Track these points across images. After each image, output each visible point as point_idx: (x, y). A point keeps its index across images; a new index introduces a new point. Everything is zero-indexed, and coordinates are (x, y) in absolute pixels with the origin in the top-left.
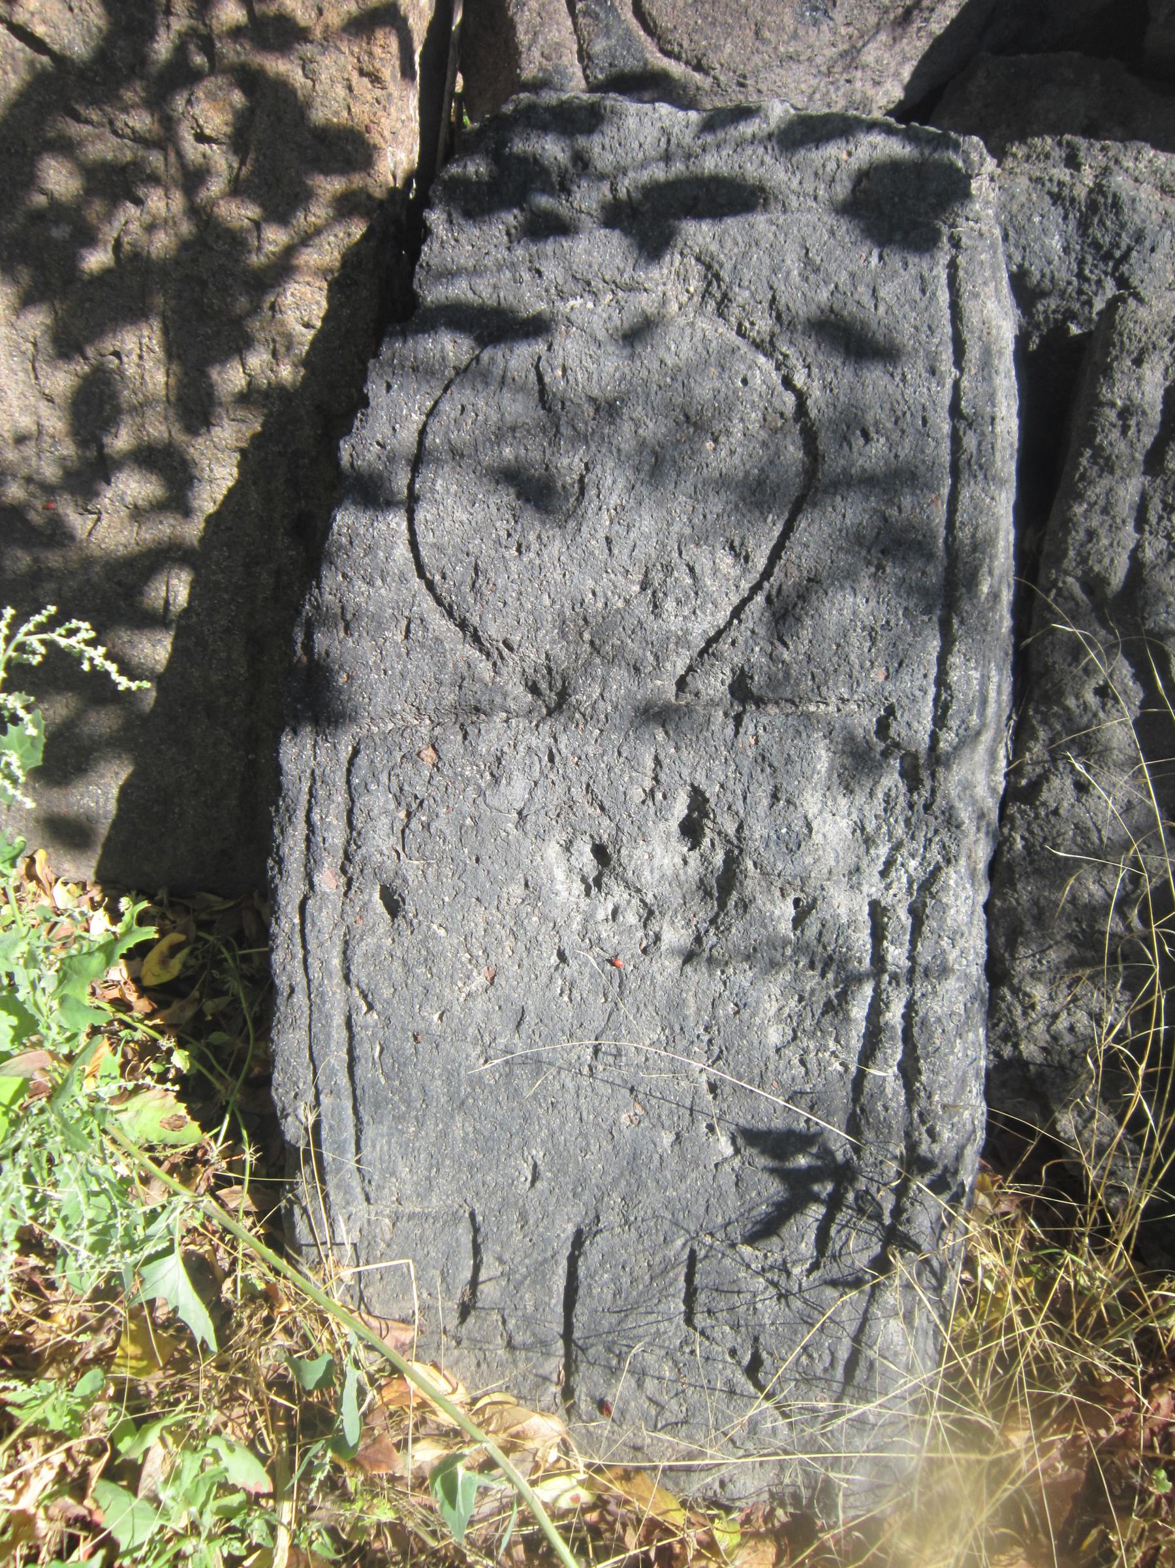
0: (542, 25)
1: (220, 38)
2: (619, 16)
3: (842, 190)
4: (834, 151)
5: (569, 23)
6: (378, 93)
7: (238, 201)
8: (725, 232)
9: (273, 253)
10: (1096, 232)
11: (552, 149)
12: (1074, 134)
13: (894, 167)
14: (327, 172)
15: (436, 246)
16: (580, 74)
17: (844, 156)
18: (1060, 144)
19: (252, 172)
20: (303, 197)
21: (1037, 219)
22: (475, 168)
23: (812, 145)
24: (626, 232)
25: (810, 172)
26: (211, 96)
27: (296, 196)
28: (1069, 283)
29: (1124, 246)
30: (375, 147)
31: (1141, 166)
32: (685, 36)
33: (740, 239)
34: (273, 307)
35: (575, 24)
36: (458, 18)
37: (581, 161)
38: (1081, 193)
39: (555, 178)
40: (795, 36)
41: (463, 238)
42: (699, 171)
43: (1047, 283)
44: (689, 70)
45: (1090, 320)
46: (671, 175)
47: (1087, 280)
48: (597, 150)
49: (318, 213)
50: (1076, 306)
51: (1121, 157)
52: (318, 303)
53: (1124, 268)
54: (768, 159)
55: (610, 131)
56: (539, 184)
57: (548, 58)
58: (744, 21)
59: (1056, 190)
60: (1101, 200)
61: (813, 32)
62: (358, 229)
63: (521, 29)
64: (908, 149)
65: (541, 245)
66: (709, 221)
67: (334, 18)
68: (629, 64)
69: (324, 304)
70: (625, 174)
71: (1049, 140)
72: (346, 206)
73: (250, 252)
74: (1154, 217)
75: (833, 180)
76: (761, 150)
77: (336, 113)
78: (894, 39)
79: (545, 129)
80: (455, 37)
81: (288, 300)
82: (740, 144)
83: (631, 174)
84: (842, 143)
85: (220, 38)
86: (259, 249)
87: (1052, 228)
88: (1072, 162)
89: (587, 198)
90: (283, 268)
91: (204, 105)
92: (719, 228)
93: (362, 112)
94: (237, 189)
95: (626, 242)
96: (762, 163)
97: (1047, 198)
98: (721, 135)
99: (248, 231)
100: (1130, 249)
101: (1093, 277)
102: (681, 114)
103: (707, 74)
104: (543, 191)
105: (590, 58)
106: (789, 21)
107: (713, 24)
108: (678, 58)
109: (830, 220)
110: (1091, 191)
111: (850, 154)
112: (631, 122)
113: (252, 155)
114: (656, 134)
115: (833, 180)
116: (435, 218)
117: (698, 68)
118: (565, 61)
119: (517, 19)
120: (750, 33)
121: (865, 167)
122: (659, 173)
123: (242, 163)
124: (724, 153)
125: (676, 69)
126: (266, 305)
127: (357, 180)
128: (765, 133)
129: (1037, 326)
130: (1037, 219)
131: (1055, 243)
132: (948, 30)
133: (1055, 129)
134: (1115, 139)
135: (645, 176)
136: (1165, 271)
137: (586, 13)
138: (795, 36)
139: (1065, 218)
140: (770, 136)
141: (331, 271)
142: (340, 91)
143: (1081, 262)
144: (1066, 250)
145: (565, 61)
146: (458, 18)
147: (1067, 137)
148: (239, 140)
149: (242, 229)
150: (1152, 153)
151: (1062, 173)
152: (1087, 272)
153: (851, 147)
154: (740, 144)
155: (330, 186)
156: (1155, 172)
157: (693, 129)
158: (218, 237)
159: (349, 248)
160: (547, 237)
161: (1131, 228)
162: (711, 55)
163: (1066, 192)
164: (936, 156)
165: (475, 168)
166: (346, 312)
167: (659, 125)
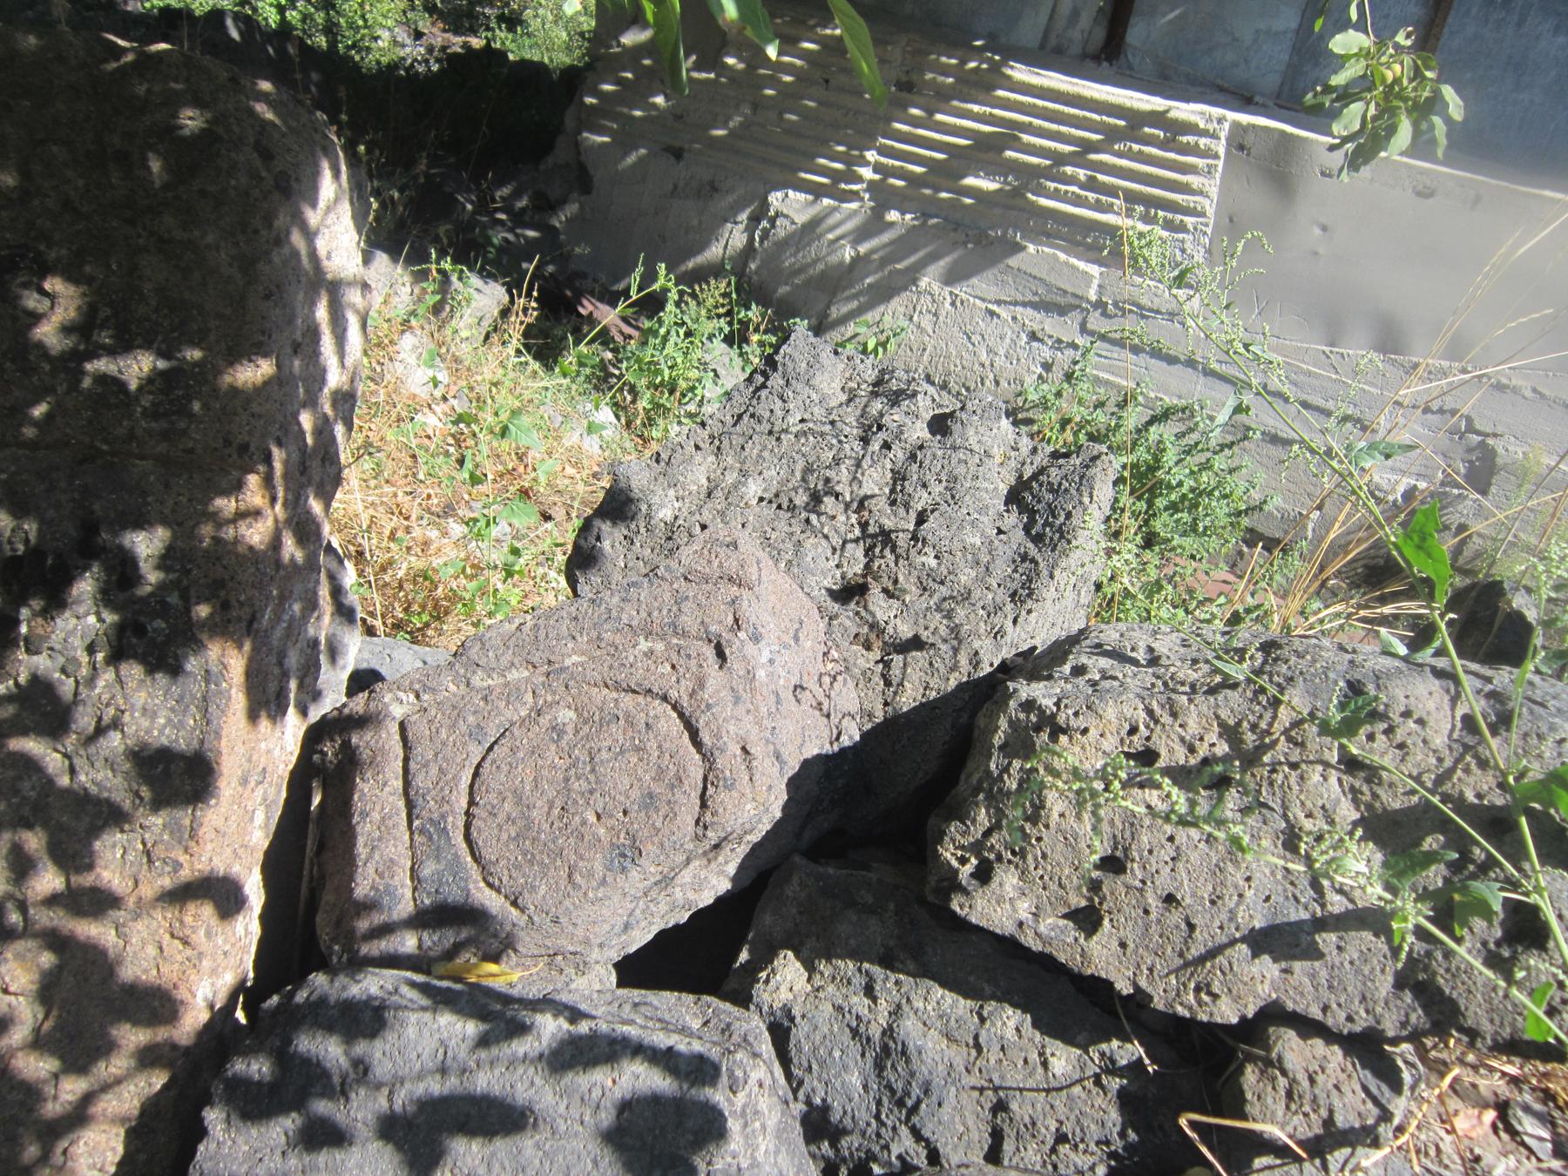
0: (380, 839)
1: (35, 905)
2: (449, 839)
3: (607, 1118)
4: (600, 1077)
5: (407, 837)
6: (189, 952)
7: (37, 1054)
8: (493, 1154)
9: (70, 1103)
10: (889, 1073)
11: (331, 1051)
12: (872, 962)
13: (654, 1101)
14: (136, 1023)
15: (213, 1146)
16: (408, 894)
17: (610, 1083)
18: (860, 970)
19: (54, 1028)
20: (106, 1048)
21: (837, 1054)
22: (257, 1068)
23: (580, 1068)
24: (399, 1147)
25: (577, 1097)
26: (19, 957)
27: (98, 1049)
28: (868, 1124)
29: (914, 1098)
30: (182, 1002)
31: (929, 1008)
32: (506, 872)
33: (507, 1163)
34: (65, 1152)
35: (412, 840)
36: (316, 800)
37: (362, 1068)
38: (875, 1032)
39: (336, 1080)
40: (603, 882)
41: (240, 1140)
42: (472, 1088)
43: (848, 1122)
44: (508, 904)
45: (890, 1163)
46: (446, 1091)
47: (884, 1124)
48: (378, 1055)
49: (118, 1064)
50: (876, 1149)
51: (913, 996)
52: (113, 1149)
53: (915, 1119)
54: (538, 1081)
55: (391, 1036)
56: (319, 1089)
57: (381, 876)
58: (559, 863)
59: (854, 1024)
60: (892, 1045)
61: (620, 878)
62: (158, 1080)
63: (361, 841)
64: (668, 1081)
65: (313, 1156)
66: (480, 1140)
67: (147, 891)
68: (453, 894)
69: (120, 1150)
70: (402, 1084)
71: (851, 965)
72: (148, 1058)
73: (45, 1100)
74: (940, 1068)
75: (598, 1107)
76: (532, 1070)
77: (146, 971)
78: (709, 861)
79: (330, 1028)
80: (313, 816)
81: (80, 1149)
82: (512, 1063)
83: (408, 1085)
84: (606, 1069)
85: (35, 905)
86: (55, 1098)
87: (852, 1064)
88: (869, 991)
89: (361, 1111)
90: (79, 1116)
91: (12, 965)
92: (487, 1151)
93: (169, 974)
94: (38, 1043)
95: (397, 1158)
96: (532, 1083)
97: (847, 1030)
98: (495, 1051)
99: (45, 1082)
100: (919, 1102)
101: (889, 1123)
102: (459, 1025)
103: (523, 911)
104: (323, 1095)
105: (419, 881)
106: (598, 867)
107: (531, 862)
108: (498, 891)
109: (595, 1147)
110: (884, 1033)
111: (614, 1081)
112: (411, 1032)
113: (55, 1013)
114: (434, 1044)
115: (598, 1107)
116: (213, 1117)
117: (514, 904)
118: (396, 881)
119: (359, 829)
120: (564, 874)
121: (628, 1096)
122: (435, 1087)
123: (46, 1017)
124: (497, 1072)
125: (493, 902)
126: (59, 1150)
127: (162, 1034)
128: (536, 1053)
129: (844, 1160)
130: (837, 1054)
131: (855, 1080)
132: (764, 838)
133: (857, 955)
134: (908, 974)
135: (420, 1089)
136: (954, 1123)
137: (422, 831)
138: (603, 882)
139: (863, 1055)
140: (541, 1056)
141: (129, 1120)
142: (152, 951)
143: (879, 1103)
144: (865, 1087)
145: (396, 881)
146: (316, 800)
147: (866, 965)
148: (47, 992)
149: (38, 1081)
150: (940, 992)
151: (860, 1003)
152: (883, 1116)
153: (616, 1074)
154: (512, 1063)
155: (132, 1037)
156: (941, 1017)
157: (470, 1043)
158: (12, 1088)
159: (148, 1099)
160: (321, 1148)
161: (920, 1078)
162: (527, 895)
163: (862, 1029)
164: (693, 1091)
165: (257, 1068)
166: (142, 1157)
167: (437, 1036)
